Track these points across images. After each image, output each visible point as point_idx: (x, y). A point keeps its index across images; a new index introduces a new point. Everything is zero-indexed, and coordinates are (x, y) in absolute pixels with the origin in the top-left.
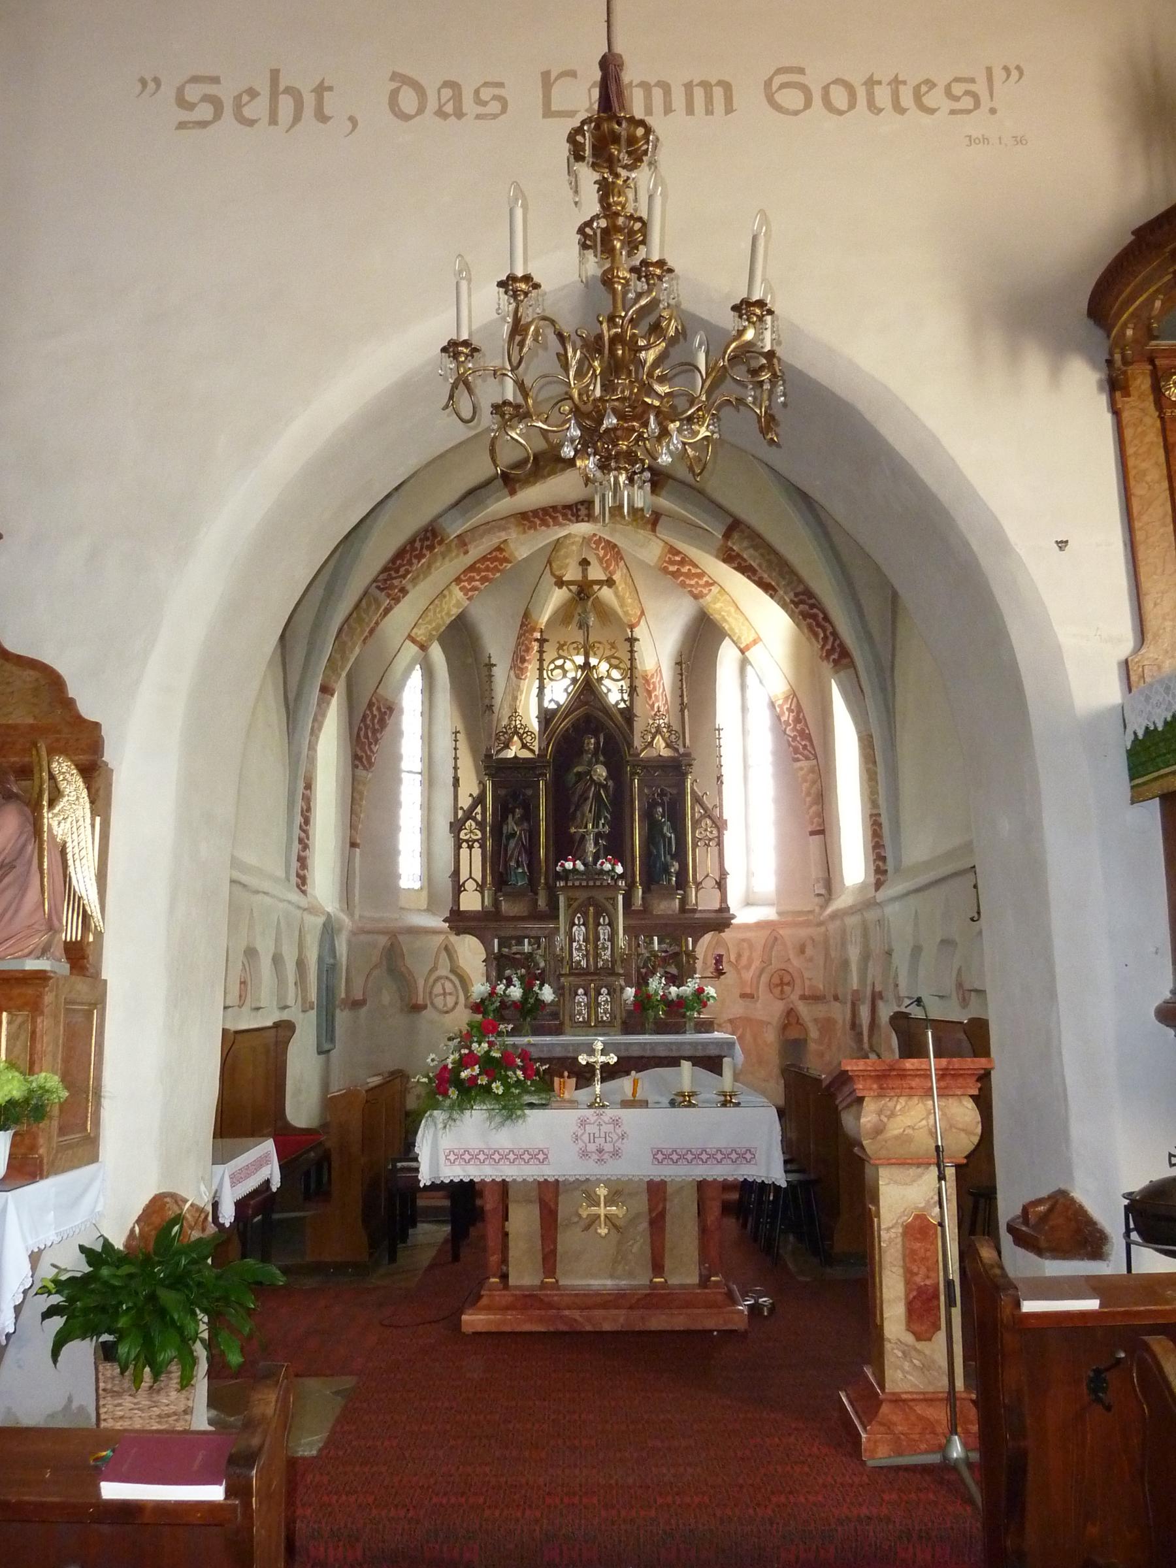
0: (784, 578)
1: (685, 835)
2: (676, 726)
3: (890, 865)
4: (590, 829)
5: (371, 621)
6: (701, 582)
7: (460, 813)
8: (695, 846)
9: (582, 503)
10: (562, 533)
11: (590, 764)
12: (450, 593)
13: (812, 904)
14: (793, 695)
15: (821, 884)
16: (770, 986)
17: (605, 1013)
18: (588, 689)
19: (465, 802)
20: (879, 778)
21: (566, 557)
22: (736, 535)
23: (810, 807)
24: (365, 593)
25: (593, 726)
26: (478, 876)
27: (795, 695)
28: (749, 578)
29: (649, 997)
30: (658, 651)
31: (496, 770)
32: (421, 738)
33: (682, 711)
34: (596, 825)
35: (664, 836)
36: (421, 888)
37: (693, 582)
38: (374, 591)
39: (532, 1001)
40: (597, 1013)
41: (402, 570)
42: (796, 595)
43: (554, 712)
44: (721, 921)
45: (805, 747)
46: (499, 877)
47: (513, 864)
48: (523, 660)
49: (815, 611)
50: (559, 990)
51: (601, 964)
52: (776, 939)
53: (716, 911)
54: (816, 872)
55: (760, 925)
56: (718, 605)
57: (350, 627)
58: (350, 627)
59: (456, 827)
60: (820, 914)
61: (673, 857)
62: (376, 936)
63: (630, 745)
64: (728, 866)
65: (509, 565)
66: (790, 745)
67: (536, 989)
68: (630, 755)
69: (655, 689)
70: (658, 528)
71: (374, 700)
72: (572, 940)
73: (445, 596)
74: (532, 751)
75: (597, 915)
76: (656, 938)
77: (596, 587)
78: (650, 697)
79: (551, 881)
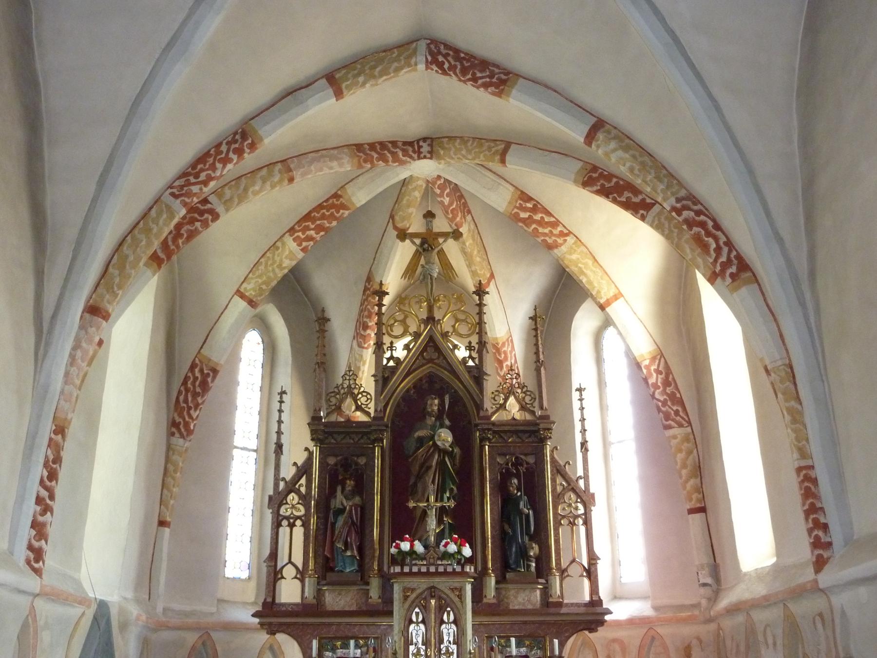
0: (661, 181)
2: (531, 386)
3: (836, 535)
4: (432, 503)
5: (160, 231)
6: (556, 232)
7: (282, 485)
8: (558, 524)
9: (425, 139)
10: (403, 173)
11: (433, 428)
12: (284, 244)
14: (659, 355)
15: (706, 572)
18: (432, 348)
19: (288, 472)
20: (807, 420)
21: (409, 206)
22: (601, 136)
23: (686, 482)
25: (437, 386)
26: (299, 562)
27: (662, 355)
28: (615, 201)
30: (508, 320)
31: (323, 432)
32: (259, 413)
33: (538, 371)
35: (521, 513)
36: (249, 578)
37: (546, 231)
38: (167, 198)
42: (678, 200)
43: (393, 370)
44: (592, 617)
45: (677, 413)
46: (325, 566)
47: (340, 545)
48: (366, 327)
49: (702, 218)
52: (653, 638)
54: (700, 557)
55: (632, 622)
56: (574, 257)
59: (276, 501)
60: (709, 608)
61: (532, 538)
63: (479, 406)
64: (598, 549)
65: (347, 213)
66: (659, 410)
68: (481, 418)
69: (506, 359)
70: (508, 158)
71: (197, 361)
72: (408, 642)
73: (278, 248)
74: (368, 414)
75: (441, 609)
76: (513, 640)
77: (441, 240)
78: (502, 368)
79: (385, 568)
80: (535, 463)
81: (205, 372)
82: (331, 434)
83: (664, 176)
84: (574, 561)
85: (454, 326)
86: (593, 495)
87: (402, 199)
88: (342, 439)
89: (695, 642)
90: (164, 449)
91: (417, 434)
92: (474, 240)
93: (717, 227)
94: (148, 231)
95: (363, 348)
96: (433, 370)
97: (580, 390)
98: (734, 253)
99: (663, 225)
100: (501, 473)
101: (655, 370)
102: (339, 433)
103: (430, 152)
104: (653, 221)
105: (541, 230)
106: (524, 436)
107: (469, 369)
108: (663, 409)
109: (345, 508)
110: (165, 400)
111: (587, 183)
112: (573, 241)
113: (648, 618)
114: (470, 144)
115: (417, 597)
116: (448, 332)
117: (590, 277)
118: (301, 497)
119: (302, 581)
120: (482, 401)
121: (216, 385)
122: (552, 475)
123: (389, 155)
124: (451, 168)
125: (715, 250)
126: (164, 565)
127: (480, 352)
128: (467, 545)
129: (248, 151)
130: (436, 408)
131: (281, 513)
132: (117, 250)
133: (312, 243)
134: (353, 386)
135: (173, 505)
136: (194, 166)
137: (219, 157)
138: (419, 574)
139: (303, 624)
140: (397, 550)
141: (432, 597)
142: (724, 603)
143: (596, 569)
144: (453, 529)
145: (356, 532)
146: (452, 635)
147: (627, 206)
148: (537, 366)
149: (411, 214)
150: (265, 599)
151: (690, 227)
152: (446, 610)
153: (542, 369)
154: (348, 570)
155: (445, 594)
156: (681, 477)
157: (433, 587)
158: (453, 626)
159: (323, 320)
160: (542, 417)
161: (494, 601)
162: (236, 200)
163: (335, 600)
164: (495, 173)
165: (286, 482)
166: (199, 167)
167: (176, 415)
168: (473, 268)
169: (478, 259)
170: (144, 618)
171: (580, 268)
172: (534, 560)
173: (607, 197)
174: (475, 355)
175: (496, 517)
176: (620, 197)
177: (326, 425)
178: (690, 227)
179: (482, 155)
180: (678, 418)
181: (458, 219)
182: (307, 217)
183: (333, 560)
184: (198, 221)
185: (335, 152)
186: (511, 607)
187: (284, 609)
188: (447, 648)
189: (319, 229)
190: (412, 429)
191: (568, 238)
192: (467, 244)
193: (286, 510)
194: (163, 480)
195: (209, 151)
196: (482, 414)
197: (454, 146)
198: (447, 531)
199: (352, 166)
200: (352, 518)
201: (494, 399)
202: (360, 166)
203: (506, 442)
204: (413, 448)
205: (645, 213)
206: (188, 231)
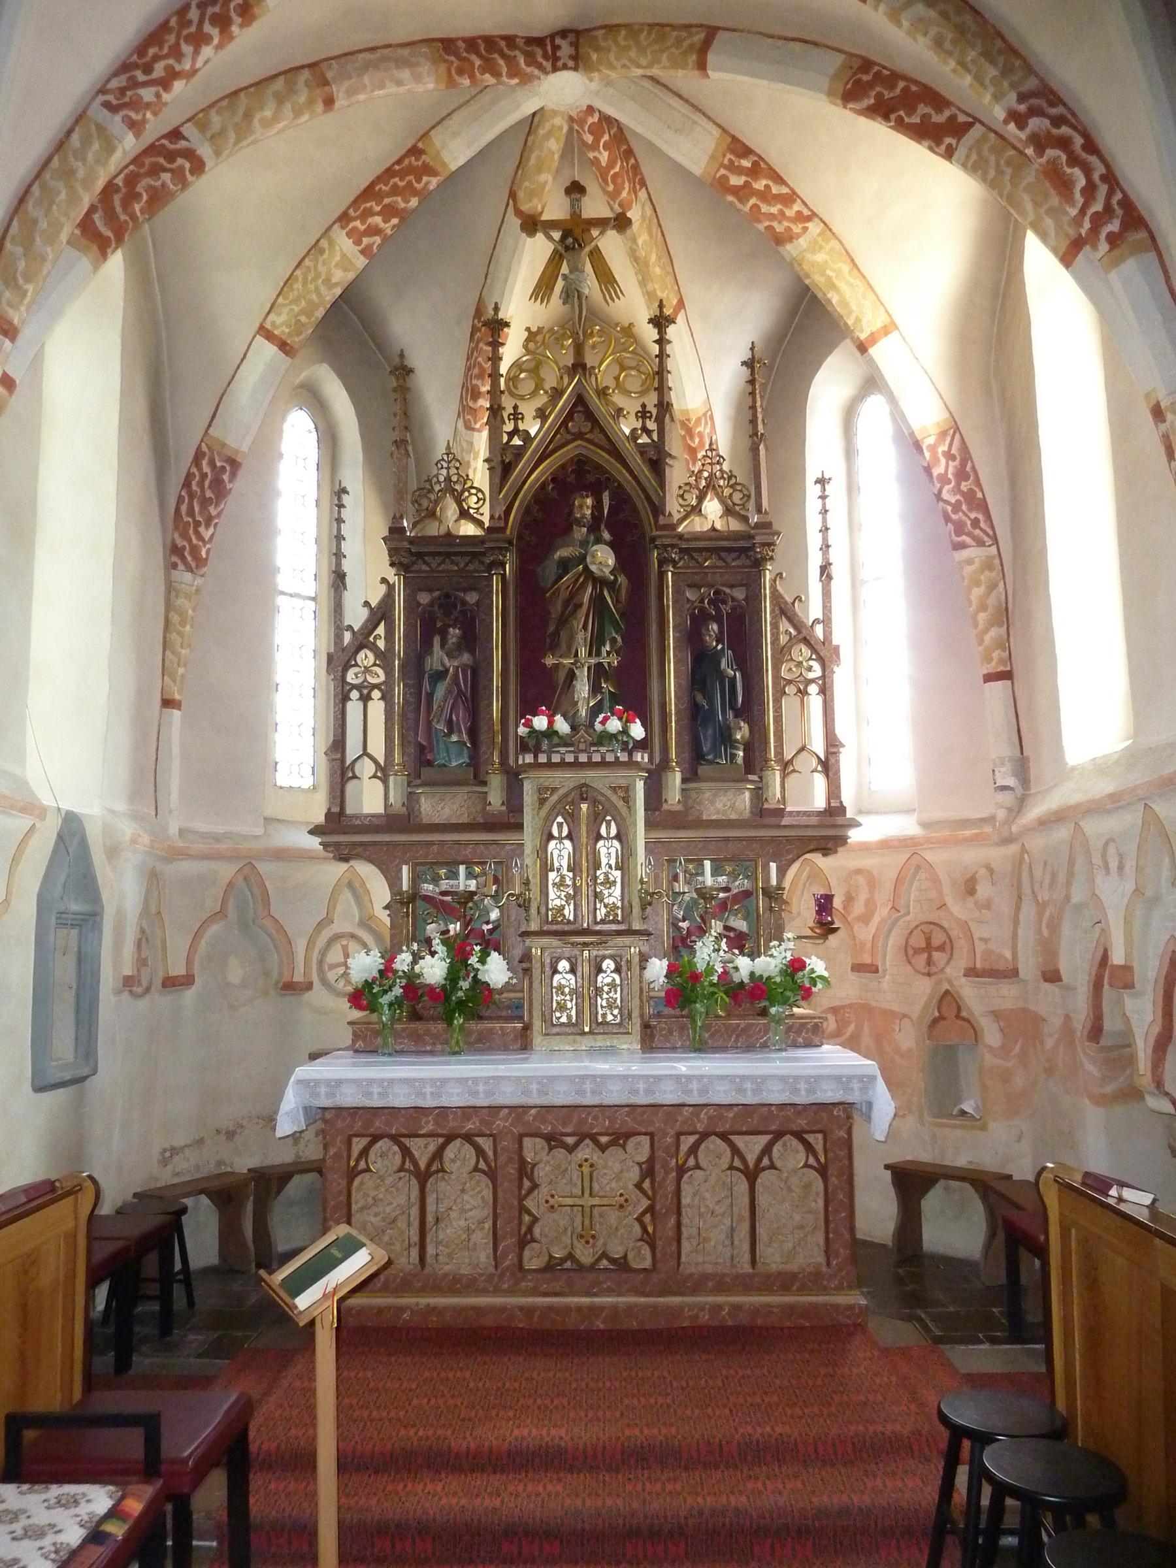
0: (992, 62)
1: (760, 671)
4: (581, 659)
6: (790, 213)
7: (347, 636)
8: (780, 693)
9: (563, 33)
11: (584, 544)
12: (332, 243)
13: (996, 805)
14: (953, 429)
16: (908, 952)
17: (610, 1006)
19: (356, 616)
21: (539, 170)
24: (80, 118)
26: (377, 747)
27: (957, 429)
28: (901, 126)
29: (695, 977)
31: (410, 552)
33: (755, 450)
34: (595, 648)
35: (721, 676)
37: (774, 210)
38: (98, 113)
39: (465, 984)
40: (593, 1006)
41: (159, 70)
42: (1022, 98)
43: (519, 452)
44: (828, 832)
45: (975, 523)
46: (419, 761)
47: (441, 726)
49: (1065, 130)
50: (523, 965)
51: (601, 913)
52: (918, 867)
53: (819, 813)
54: (1001, 747)
55: (886, 845)
56: (820, 257)
57: (43, 187)
58: (43, 187)
59: (338, 661)
60: (1008, 822)
61: (738, 714)
62: (214, 865)
63: (658, 509)
64: (842, 731)
65: (434, 182)
66: (947, 519)
67: (473, 960)
70: (711, 58)
71: (204, 448)
72: (546, 867)
73: (322, 251)
74: (479, 523)
75: (597, 818)
76: (707, 864)
77: (595, 233)
80: (746, 599)
81: (218, 464)
82: (420, 555)
83: (1000, 52)
84: (803, 749)
85: (617, 378)
86: (837, 648)
87: (529, 157)
88: (439, 565)
89: (982, 872)
90: (163, 589)
91: (559, 554)
92: (651, 236)
93: (1091, 146)
94: (68, 174)
95: (473, 429)
96: (584, 452)
97: (822, 481)
98: (1119, 196)
99: (987, 161)
100: (692, 615)
101: (944, 453)
102: (434, 554)
103: (572, 57)
104: (968, 157)
105: (765, 208)
106: (729, 558)
107: (642, 450)
108: (954, 517)
109: (447, 670)
110: (155, 503)
111: (851, 93)
112: (818, 231)
113: (912, 838)
114: (642, 37)
115: (560, 801)
116: (607, 388)
117: (847, 298)
118: (378, 653)
119: (385, 781)
120: (663, 500)
121: (238, 487)
122: (772, 618)
123: (501, 62)
124: (611, 91)
125: (1084, 191)
126: (176, 766)
127: (660, 421)
128: (637, 720)
129: (239, 20)
130: (589, 512)
131: (349, 680)
132: (16, 211)
133: (378, 240)
134: (454, 478)
135: (182, 676)
136: (141, 50)
137: (185, 32)
138: (563, 765)
139: (388, 844)
140: (527, 730)
141: (584, 799)
142: (1036, 811)
143: (838, 761)
144: (614, 698)
145: (466, 709)
146: (613, 856)
147: (926, 133)
148: (754, 443)
149: (546, 182)
150: (329, 809)
151: (1040, 149)
152: (604, 819)
153: (762, 447)
154: (454, 764)
155: (603, 795)
156: (976, 625)
157: (585, 785)
158: (616, 843)
159: (403, 371)
160: (758, 526)
161: (679, 808)
162: (232, 136)
163: (436, 807)
164: (687, 101)
165: (354, 632)
166: (152, 51)
167: (176, 535)
168: (650, 287)
169: (658, 270)
170: (146, 839)
171: (829, 278)
172: (742, 747)
173: (886, 118)
174: (651, 425)
175: (684, 683)
176: (909, 115)
177: (412, 541)
178: (1040, 149)
179: (664, 57)
180: (977, 532)
181: (624, 194)
182: (368, 193)
183: (432, 750)
184: (165, 170)
185: (406, 52)
186: (705, 818)
187: (358, 822)
188: (606, 874)
189: (389, 212)
190: (550, 548)
191: (809, 225)
192: (640, 242)
193: (356, 675)
194: (165, 638)
195: (167, 22)
196: (662, 521)
197: (617, 44)
198: (607, 704)
199: (437, 82)
200: (458, 684)
201: (682, 496)
202: (451, 83)
203: (701, 566)
204: (553, 577)
205: (954, 142)
206: (150, 188)
